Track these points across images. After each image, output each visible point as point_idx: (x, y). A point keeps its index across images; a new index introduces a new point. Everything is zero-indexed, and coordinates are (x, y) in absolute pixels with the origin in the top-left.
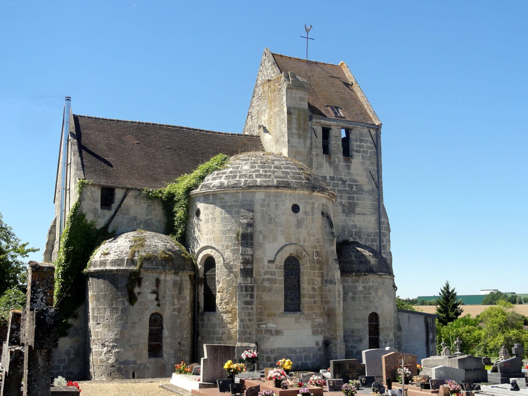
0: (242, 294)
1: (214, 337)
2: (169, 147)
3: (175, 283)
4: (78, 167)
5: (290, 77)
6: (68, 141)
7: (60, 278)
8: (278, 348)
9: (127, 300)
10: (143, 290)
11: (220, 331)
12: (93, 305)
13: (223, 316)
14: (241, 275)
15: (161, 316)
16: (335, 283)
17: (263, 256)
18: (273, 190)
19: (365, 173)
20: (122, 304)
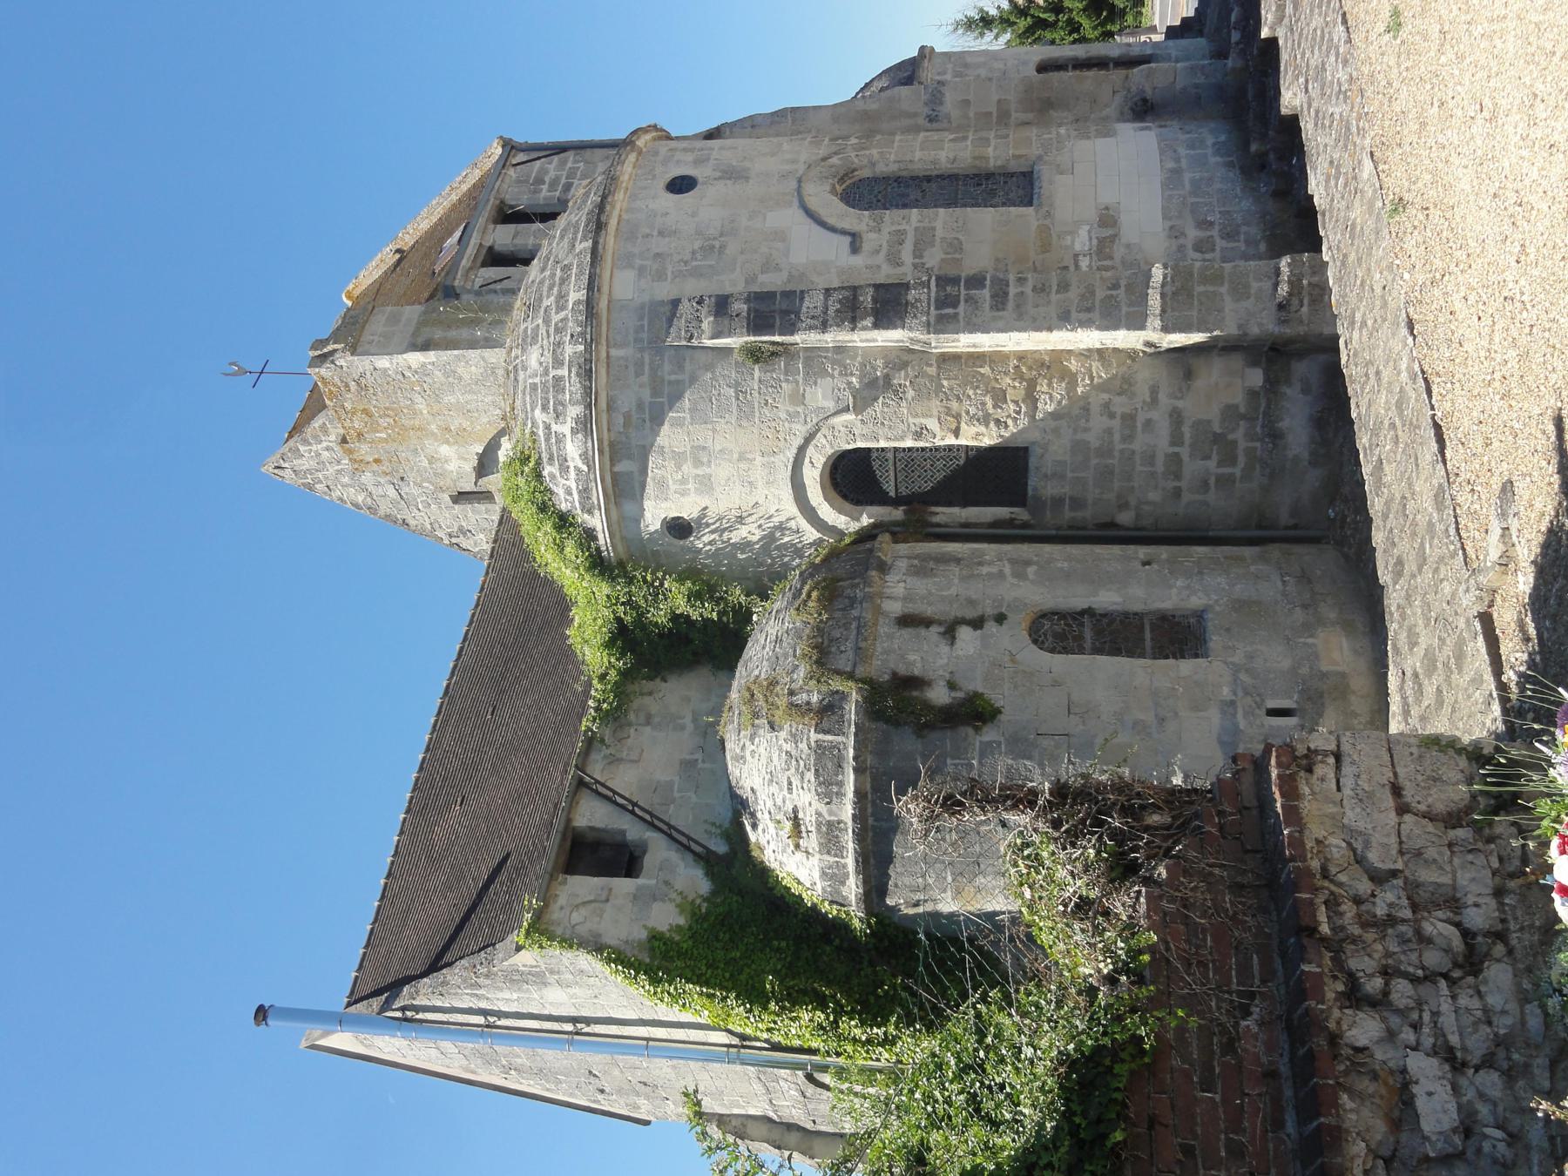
1: (1122, 451)
2: (490, 710)
5: (325, 350)
6: (406, 1020)
9: (977, 729)
10: (941, 673)
11: (1098, 422)
12: (994, 888)
14: (899, 322)
15: (1044, 616)
17: (833, 270)
18: (610, 240)
20: (993, 754)
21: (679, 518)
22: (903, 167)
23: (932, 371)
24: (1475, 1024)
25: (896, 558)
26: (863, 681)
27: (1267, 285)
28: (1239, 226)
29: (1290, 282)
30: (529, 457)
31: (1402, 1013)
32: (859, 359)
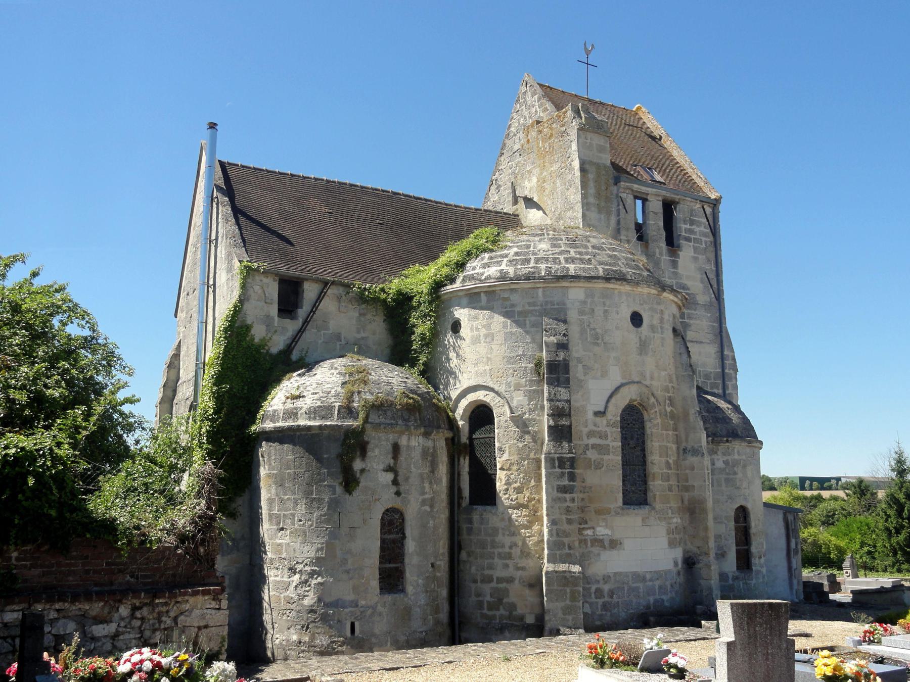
0: (554, 472)
1: (494, 553)
2: (381, 222)
3: (425, 453)
4: (235, 241)
5: (582, 113)
6: (212, 200)
7: (204, 443)
8: (615, 574)
9: (341, 484)
10: (369, 465)
11: (507, 541)
13: (512, 514)
14: (551, 438)
15: (402, 515)
16: (703, 453)
17: (584, 403)
18: (600, 285)
19: (698, 276)
20: (330, 491)
21: (461, 327)
22: (649, 436)
23: (532, 455)
24: (126, 644)
25: (434, 441)
26: (363, 428)
27: (570, 623)
28: (610, 611)
31: (130, 623)
32: (538, 418)
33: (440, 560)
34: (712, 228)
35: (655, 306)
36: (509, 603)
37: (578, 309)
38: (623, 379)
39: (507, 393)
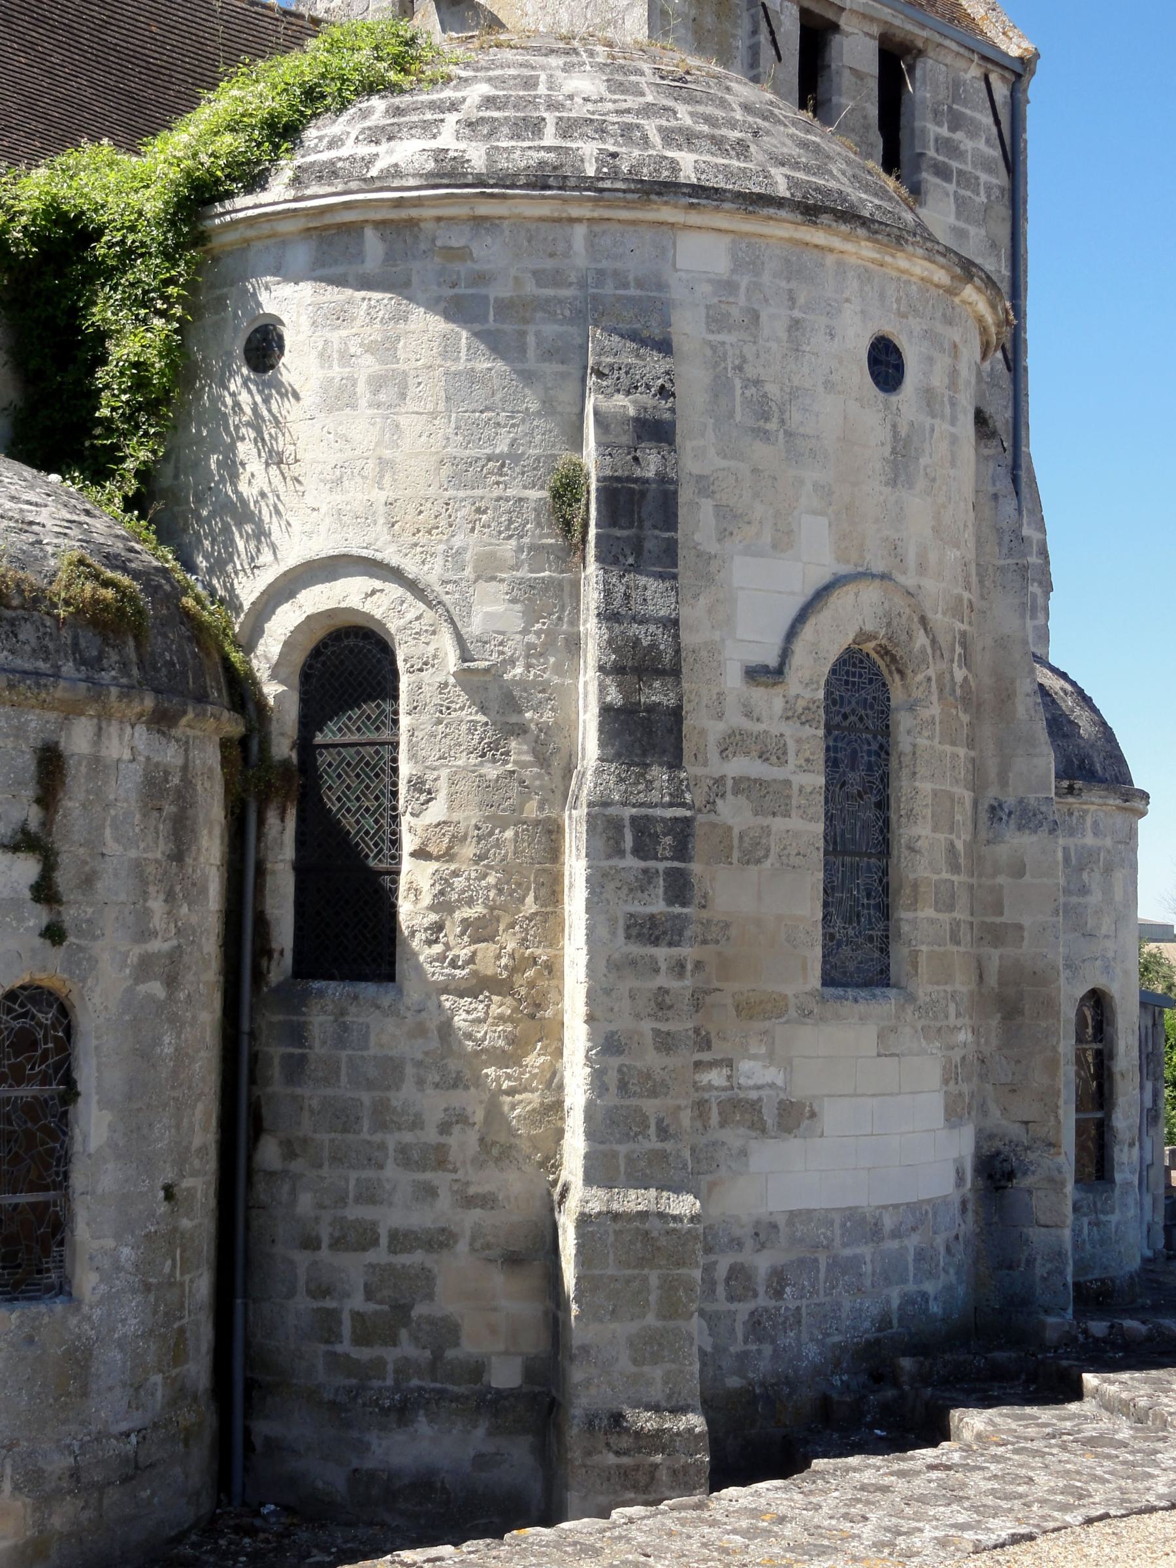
1: (382, 1146)
8: (792, 1215)
14: (611, 751)
17: (717, 636)
21: (281, 347)
22: (906, 760)
23: (531, 810)
25: (186, 745)
27: (656, 1393)
28: (773, 1341)
29: (660, 1432)
30: (407, 72)
32: (556, 680)
33: (194, 1174)
34: (1008, 148)
35: (940, 328)
36: (431, 1321)
37: (708, 307)
38: (838, 560)
39: (450, 587)
